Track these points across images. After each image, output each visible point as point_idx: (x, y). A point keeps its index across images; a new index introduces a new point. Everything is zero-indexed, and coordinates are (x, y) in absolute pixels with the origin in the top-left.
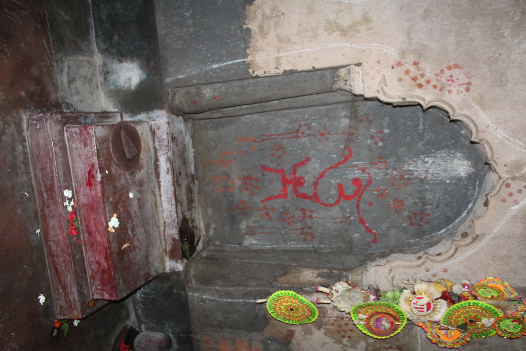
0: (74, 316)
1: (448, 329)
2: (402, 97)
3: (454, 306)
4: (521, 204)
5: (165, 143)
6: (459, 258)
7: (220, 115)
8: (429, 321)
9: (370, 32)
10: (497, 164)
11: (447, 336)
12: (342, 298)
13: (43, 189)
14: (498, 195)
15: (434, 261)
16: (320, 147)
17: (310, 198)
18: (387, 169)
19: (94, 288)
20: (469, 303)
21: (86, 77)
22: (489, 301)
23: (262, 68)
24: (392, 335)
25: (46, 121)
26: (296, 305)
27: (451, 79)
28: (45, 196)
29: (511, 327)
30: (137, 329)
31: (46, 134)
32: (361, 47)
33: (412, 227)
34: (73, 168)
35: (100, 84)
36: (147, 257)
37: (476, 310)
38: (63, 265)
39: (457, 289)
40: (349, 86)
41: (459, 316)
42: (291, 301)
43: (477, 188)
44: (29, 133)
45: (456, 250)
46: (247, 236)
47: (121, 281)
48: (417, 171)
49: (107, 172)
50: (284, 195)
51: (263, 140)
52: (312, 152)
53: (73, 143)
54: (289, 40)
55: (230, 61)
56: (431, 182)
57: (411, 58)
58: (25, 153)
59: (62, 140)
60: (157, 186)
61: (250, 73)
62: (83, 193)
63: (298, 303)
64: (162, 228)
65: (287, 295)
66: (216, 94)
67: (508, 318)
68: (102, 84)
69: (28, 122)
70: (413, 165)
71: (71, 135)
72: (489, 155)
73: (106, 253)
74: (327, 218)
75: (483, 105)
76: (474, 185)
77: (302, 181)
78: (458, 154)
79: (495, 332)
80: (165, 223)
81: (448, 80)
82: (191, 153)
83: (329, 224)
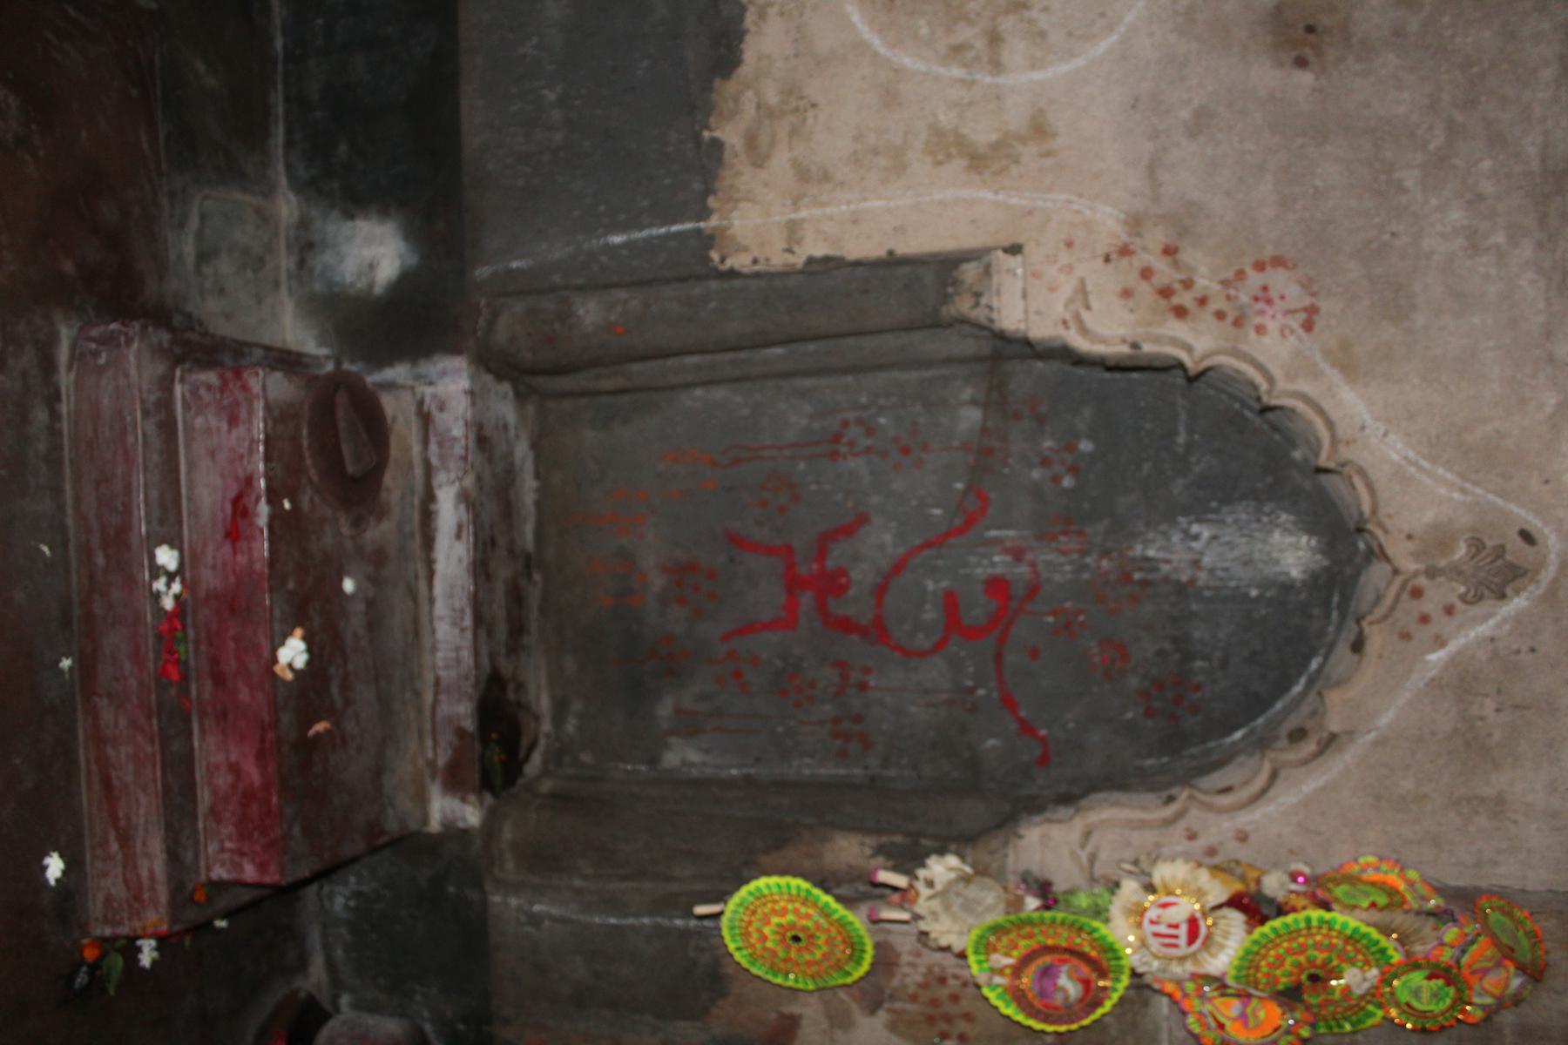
0: (144, 928)
1: (1249, 996)
2: (1130, 339)
3: (1266, 929)
4: (1452, 647)
5: (458, 450)
6: (1281, 800)
7: (620, 382)
8: (1194, 977)
9: (1049, 162)
10: (1386, 531)
11: (1245, 1024)
12: (948, 907)
13: (96, 540)
14: (1390, 620)
15: (1210, 808)
16: (898, 485)
17: (863, 631)
18: (1084, 553)
19: (212, 848)
20: (1308, 920)
21: (246, 251)
22: (1364, 915)
23: (746, 249)
24: (1086, 1022)
25: (129, 342)
26: (809, 924)
27: (1264, 296)
28: (100, 560)
29: (1425, 995)
30: (327, 1006)
31: (122, 382)
32: (1023, 202)
33: (1150, 723)
34: (191, 487)
35: (283, 277)
36: (378, 773)
37: (1326, 942)
38: (131, 767)
39: (1274, 884)
40: (986, 311)
41: (1280, 960)
42: (796, 911)
43: (1335, 615)
44: (72, 376)
45: (1274, 776)
46: (673, 740)
47: (297, 830)
48: (1168, 561)
49: (287, 505)
50: (788, 621)
51: (736, 462)
52: (875, 499)
53: (197, 414)
54: (826, 177)
55: (662, 226)
56: (1207, 593)
57: (1157, 237)
58: (53, 431)
59: (166, 404)
60: (422, 573)
61: (711, 260)
62: (209, 561)
63: (816, 917)
64: (429, 697)
65: (785, 890)
66: (613, 318)
67: (1416, 967)
68: (290, 277)
69: (73, 348)
70: (1158, 544)
71: (194, 392)
72: (1366, 508)
73: (262, 740)
74: (910, 692)
75: (1349, 369)
76: (1326, 604)
77: (843, 580)
78: (1284, 517)
79: (1380, 1013)
80: (437, 682)
81: (1256, 299)
82: (528, 490)
83: (913, 709)
